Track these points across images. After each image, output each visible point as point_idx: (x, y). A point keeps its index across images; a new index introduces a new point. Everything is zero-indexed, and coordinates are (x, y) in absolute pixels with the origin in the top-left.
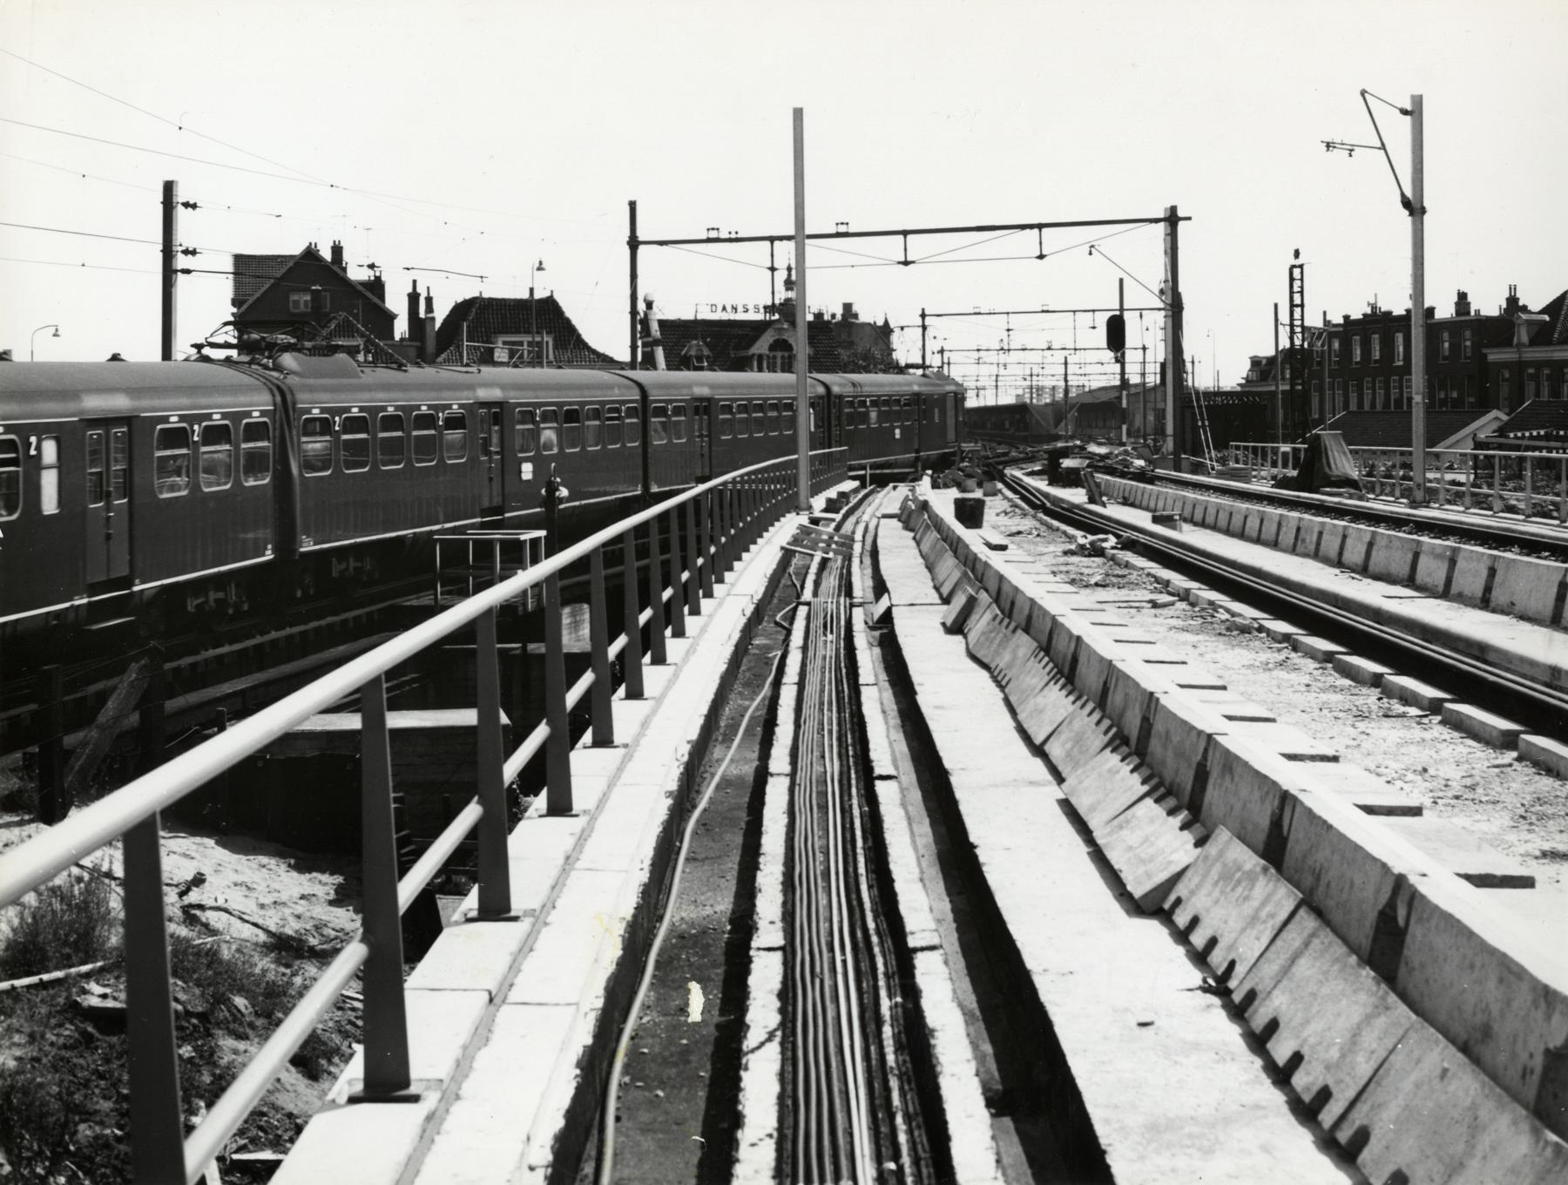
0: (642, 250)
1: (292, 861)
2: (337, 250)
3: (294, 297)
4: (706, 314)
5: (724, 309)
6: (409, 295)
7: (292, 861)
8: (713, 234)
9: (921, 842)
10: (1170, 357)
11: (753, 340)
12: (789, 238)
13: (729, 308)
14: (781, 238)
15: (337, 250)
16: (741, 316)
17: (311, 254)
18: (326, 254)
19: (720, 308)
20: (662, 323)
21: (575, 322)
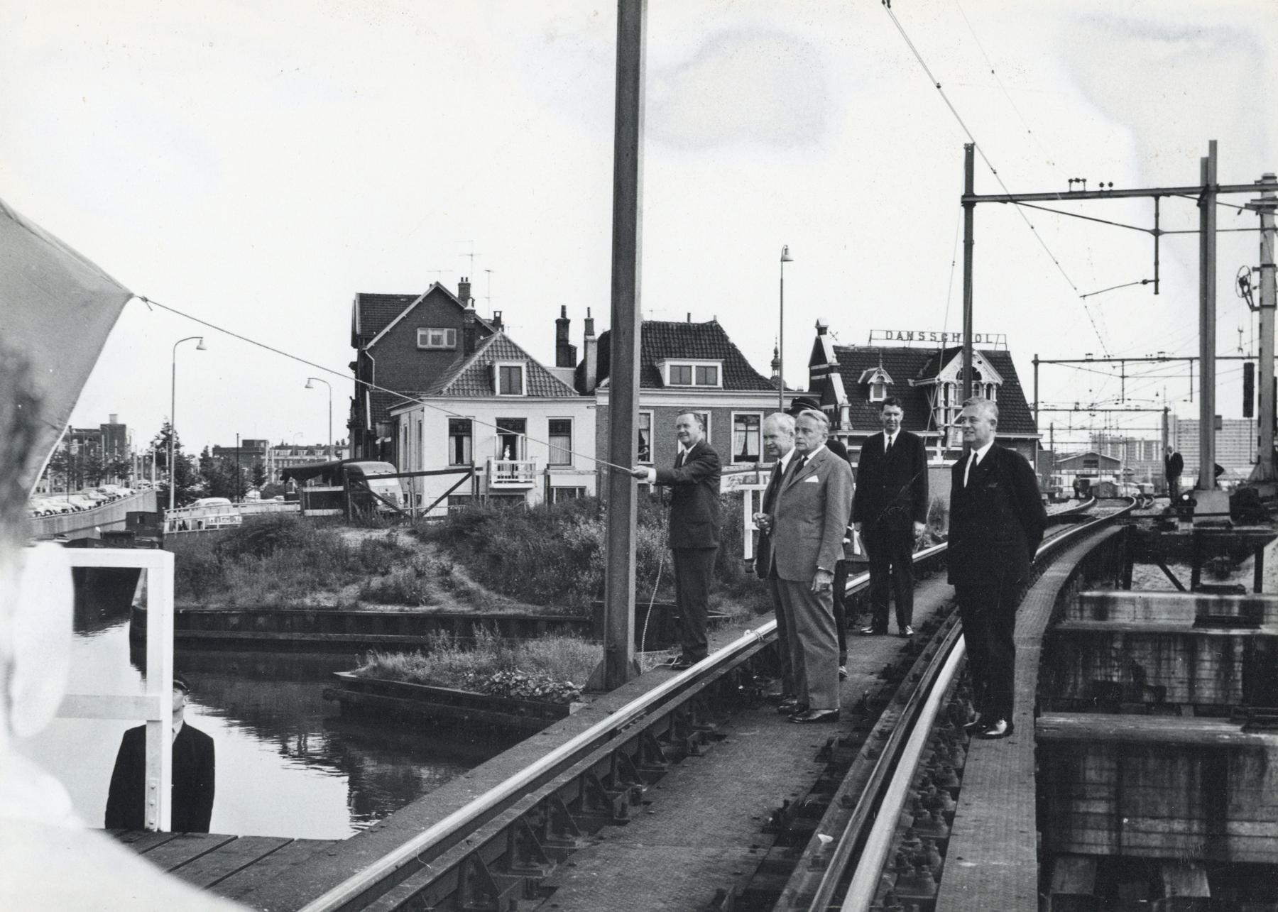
0: (979, 209)
1: (315, 743)
2: (464, 287)
3: (420, 332)
4: (880, 343)
5: (900, 337)
6: (558, 322)
7: (315, 743)
8: (1077, 187)
9: (548, 740)
10: (1211, 434)
11: (934, 371)
12: (1183, 192)
13: (905, 336)
14: (1168, 192)
15: (464, 287)
16: (915, 344)
17: (438, 292)
18: (454, 291)
19: (895, 335)
20: (837, 349)
21: (740, 347)
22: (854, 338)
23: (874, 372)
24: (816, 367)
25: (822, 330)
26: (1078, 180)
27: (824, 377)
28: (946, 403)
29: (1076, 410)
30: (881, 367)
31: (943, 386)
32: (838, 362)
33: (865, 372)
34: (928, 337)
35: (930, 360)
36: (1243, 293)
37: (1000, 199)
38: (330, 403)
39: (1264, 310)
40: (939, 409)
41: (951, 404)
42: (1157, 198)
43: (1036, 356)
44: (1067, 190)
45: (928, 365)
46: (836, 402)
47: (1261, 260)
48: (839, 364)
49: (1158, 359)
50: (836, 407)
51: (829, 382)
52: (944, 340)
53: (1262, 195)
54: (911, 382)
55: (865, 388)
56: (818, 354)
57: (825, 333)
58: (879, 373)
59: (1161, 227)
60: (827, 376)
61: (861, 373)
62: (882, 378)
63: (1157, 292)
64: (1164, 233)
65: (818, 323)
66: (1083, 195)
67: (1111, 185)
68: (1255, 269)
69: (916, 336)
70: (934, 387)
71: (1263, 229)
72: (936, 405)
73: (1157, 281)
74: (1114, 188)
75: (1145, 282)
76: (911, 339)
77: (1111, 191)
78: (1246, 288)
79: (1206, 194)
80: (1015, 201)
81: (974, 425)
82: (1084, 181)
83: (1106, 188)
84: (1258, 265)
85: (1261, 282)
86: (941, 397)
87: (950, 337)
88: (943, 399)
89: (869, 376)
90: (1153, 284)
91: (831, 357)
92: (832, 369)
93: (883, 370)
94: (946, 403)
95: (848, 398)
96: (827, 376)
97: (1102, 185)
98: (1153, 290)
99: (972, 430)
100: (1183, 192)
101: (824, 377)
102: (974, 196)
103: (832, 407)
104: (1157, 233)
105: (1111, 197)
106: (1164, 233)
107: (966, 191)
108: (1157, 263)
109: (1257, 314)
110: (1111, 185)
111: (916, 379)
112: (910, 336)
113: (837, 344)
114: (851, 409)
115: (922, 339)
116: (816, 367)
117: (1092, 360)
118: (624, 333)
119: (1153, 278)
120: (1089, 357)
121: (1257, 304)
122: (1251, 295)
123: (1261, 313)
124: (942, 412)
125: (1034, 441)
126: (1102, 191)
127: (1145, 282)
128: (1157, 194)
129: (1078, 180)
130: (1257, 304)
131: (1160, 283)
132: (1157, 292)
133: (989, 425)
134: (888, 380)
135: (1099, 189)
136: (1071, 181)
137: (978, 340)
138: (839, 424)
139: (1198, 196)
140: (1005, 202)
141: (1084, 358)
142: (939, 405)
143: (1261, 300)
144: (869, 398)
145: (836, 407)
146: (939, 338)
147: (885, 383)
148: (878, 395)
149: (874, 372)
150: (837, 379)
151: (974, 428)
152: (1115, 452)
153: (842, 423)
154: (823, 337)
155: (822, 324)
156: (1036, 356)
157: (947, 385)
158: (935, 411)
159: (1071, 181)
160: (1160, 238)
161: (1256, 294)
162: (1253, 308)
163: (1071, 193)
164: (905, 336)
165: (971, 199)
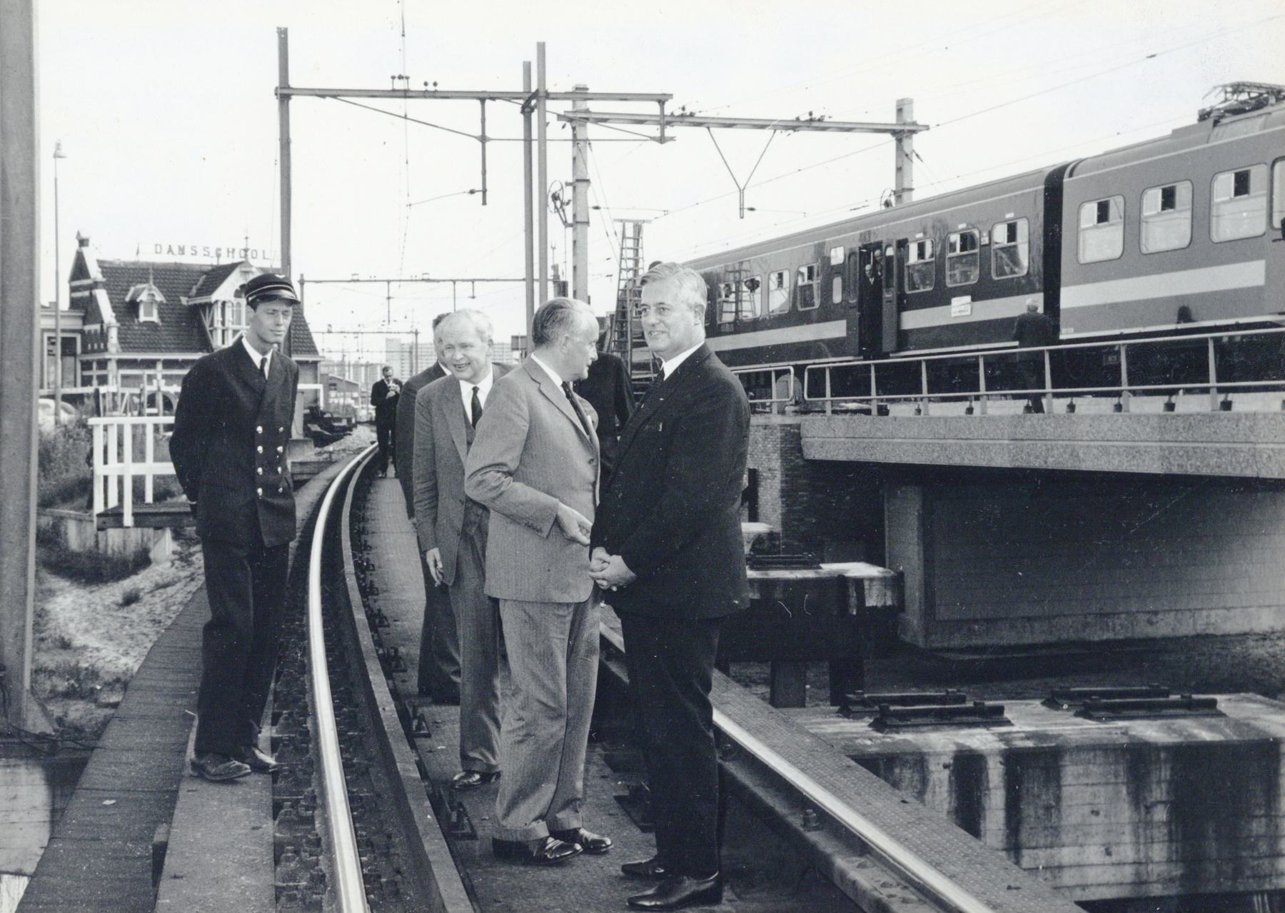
0: (295, 102)
5: (170, 250)
12: (509, 97)
13: (176, 250)
19: (165, 249)
22: (123, 254)
23: (143, 289)
24: (77, 283)
25: (83, 242)
26: (400, 77)
27: (87, 293)
28: (223, 323)
29: (329, 332)
30: (151, 282)
31: (219, 304)
32: (104, 277)
33: (132, 290)
34: (200, 251)
35: (204, 277)
36: (556, 207)
37: (318, 93)
38: (56, 180)
39: (579, 227)
40: (216, 329)
41: (228, 324)
42: (483, 100)
43: (302, 275)
44: (390, 88)
45: (200, 282)
46: (102, 322)
47: (574, 174)
48: (104, 280)
49: (423, 280)
50: (102, 327)
51: (92, 299)
52: (218, 256)
53: (574, 105)
54: (184, 300)
55: (133, 307)
56: (80, 270)
57: (87, 245)
58: (150, 290)
59: (488, 134)
60: (91, 294)
61: (128, 290)
62: (153, 295)
63: (484, 203)
64: (490, 139)
65: (78, 234)
66: (406, 94)
67: (435, 84)
68: (567, 184)
69: (188, 251)
70: (210, 306)
71: (575, 140)
72: (212, 325)
73: (484, 191)
74: (439, 88)
75: (472, 192)
76: (183, 253)
77: (436, 91)
78: (558, 203)
79: (531, 101)
80: (334, 96)
81: (664, 318)
82: (407, 78)
83: (431, 88)
84: (570, 180)
85: (575, 197)
86: (218, 317)
87: (224, 252)
88: (220, 319)
89: (138, 293)
90: (481, 194)
91: (95, 273)
92: (96, 285)
93: (154, 287)
94: (223, 323)
95: (116, 317)
96: (91, 294)
97: (426, 84)
98: (481, 201)
99: (661, 327)
100: (509, 97)
101: (87, 293)
102: (289, 88)
103: (97, 327)
104: (483, 139)
105: (435, 97)
106: (490, 139)
107: (281, 83)
108: (484, 172)
109: (570, 230)
110: (435, 84)
111: (189, 297)
112: (182, 251)
113: (101, 258)
114: (119, 329)
115: (195, 253)
116: (77, 283)
117: (358, 281)
118: (17, 201)
119: (480, 187)
120: (355, 278)
121: (570, 220)
122: (563, 211)
123: (574, 230)
124: (219, 332)
125: (315, 363)
126: (426, 91)
127: (472, 192)
128: (483, 98)
129: (400, 77)
130: (570, 220)
131: (487, 193)
132: (484, 203)
133: (691, 315)
134: (159, 297)
135: (423, 88)
136: (393, 78)
137: (254, 255)
138: (105, 346)
139: (522, 102)
140: (323, 96)
141: (350, 278)
142: (216, 325)
143: (574, 216)
144: (137, 316)
145: (102, 327)
146: (213, 253)
147: (156, 302)
148: (149, 313)
149: (143, 289)
150: (102, 297)
151: (666, 326)
152: (357, 375)
153: (109, 345)
154: (85, 250)
155: (84, 235)
156: (302, 275)
157: (224, 304)
158: (211, 331)
159: (393, 78)
160: (488, 144)
161: (569, 210)
162: (565, 223)
163: (394, 90)
164: (176, 250)
165: (286, 91)
